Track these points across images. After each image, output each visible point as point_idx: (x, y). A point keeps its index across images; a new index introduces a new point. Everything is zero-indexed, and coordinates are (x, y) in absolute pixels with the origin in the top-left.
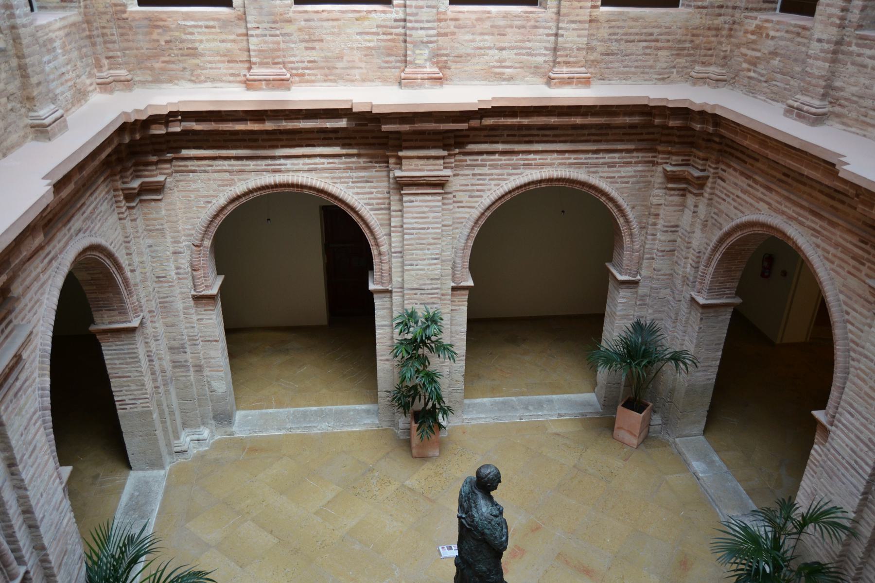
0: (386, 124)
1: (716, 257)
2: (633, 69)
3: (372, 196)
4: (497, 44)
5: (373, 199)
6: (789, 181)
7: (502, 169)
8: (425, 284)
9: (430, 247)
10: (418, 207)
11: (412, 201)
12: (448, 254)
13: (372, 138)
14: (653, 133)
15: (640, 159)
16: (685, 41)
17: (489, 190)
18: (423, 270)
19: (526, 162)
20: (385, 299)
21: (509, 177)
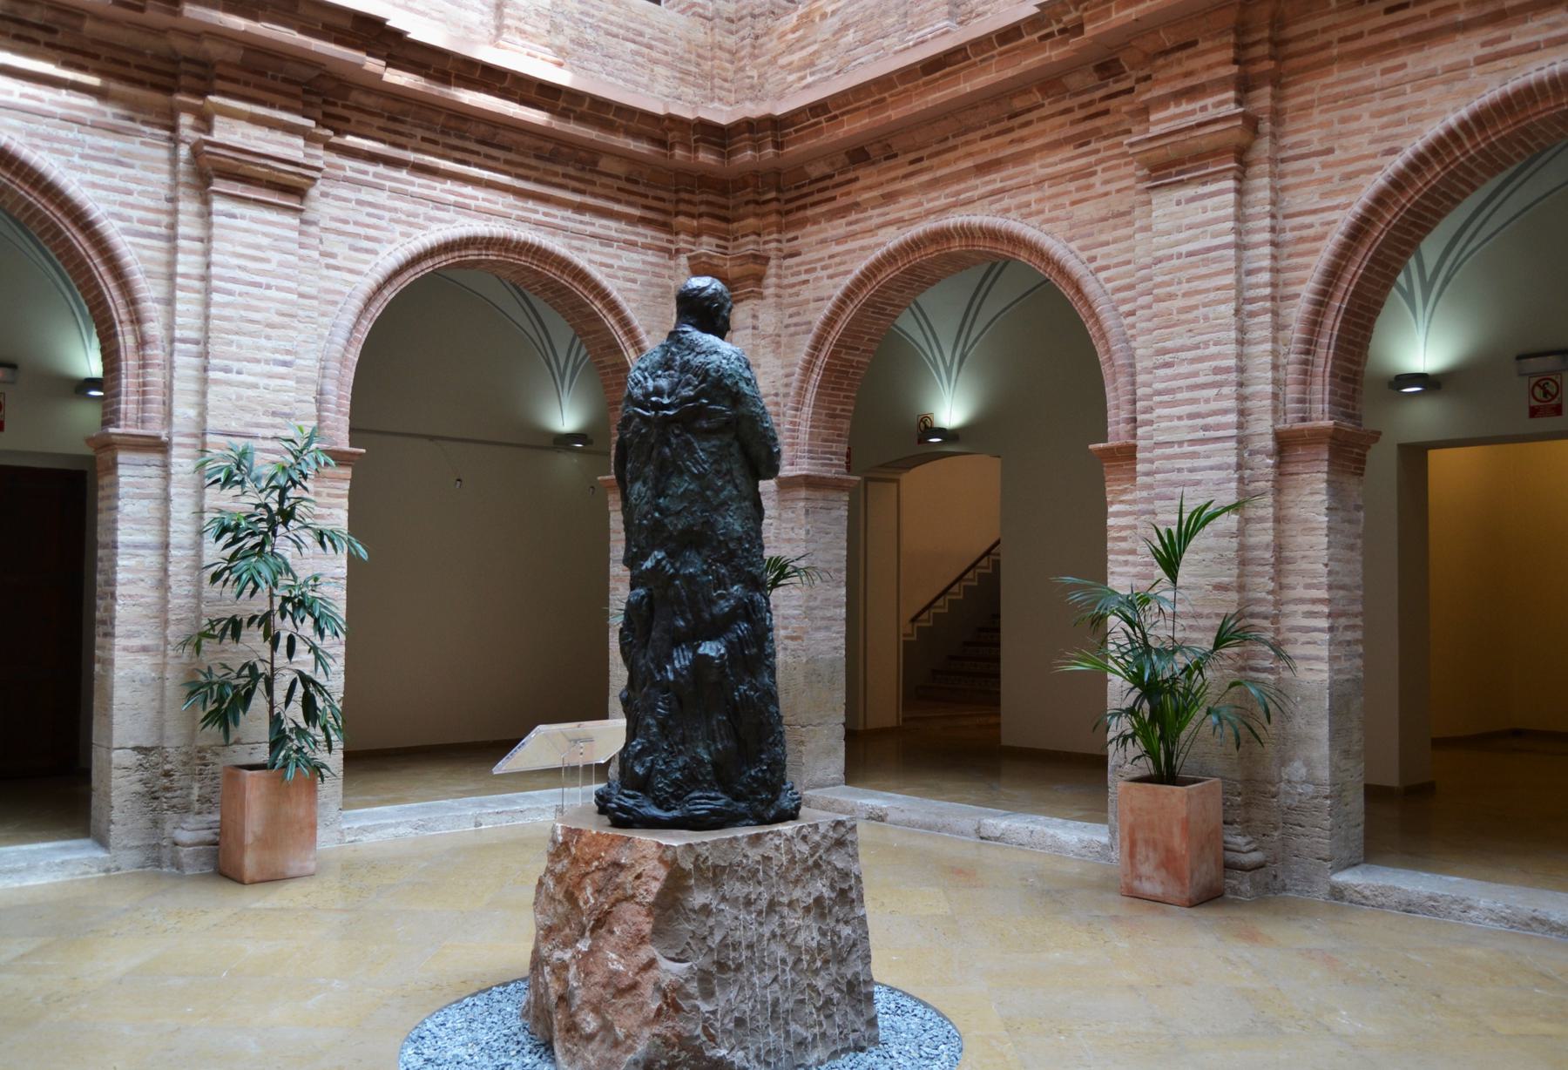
1: (812, 382)
2: (621, 83)
3: (130, 199)
5: (133, 206)
6: (926, 163)
7: (414, 202)
8: (258, 425)
10: (246, 231)
11: (233, 216)
12: (308, 363)
13: (138, 67)
15: (649, 241)
16: (689, 61)
17: (391, 242)
18: (255, 386)
20: (148, 471)
21: (428, 223)
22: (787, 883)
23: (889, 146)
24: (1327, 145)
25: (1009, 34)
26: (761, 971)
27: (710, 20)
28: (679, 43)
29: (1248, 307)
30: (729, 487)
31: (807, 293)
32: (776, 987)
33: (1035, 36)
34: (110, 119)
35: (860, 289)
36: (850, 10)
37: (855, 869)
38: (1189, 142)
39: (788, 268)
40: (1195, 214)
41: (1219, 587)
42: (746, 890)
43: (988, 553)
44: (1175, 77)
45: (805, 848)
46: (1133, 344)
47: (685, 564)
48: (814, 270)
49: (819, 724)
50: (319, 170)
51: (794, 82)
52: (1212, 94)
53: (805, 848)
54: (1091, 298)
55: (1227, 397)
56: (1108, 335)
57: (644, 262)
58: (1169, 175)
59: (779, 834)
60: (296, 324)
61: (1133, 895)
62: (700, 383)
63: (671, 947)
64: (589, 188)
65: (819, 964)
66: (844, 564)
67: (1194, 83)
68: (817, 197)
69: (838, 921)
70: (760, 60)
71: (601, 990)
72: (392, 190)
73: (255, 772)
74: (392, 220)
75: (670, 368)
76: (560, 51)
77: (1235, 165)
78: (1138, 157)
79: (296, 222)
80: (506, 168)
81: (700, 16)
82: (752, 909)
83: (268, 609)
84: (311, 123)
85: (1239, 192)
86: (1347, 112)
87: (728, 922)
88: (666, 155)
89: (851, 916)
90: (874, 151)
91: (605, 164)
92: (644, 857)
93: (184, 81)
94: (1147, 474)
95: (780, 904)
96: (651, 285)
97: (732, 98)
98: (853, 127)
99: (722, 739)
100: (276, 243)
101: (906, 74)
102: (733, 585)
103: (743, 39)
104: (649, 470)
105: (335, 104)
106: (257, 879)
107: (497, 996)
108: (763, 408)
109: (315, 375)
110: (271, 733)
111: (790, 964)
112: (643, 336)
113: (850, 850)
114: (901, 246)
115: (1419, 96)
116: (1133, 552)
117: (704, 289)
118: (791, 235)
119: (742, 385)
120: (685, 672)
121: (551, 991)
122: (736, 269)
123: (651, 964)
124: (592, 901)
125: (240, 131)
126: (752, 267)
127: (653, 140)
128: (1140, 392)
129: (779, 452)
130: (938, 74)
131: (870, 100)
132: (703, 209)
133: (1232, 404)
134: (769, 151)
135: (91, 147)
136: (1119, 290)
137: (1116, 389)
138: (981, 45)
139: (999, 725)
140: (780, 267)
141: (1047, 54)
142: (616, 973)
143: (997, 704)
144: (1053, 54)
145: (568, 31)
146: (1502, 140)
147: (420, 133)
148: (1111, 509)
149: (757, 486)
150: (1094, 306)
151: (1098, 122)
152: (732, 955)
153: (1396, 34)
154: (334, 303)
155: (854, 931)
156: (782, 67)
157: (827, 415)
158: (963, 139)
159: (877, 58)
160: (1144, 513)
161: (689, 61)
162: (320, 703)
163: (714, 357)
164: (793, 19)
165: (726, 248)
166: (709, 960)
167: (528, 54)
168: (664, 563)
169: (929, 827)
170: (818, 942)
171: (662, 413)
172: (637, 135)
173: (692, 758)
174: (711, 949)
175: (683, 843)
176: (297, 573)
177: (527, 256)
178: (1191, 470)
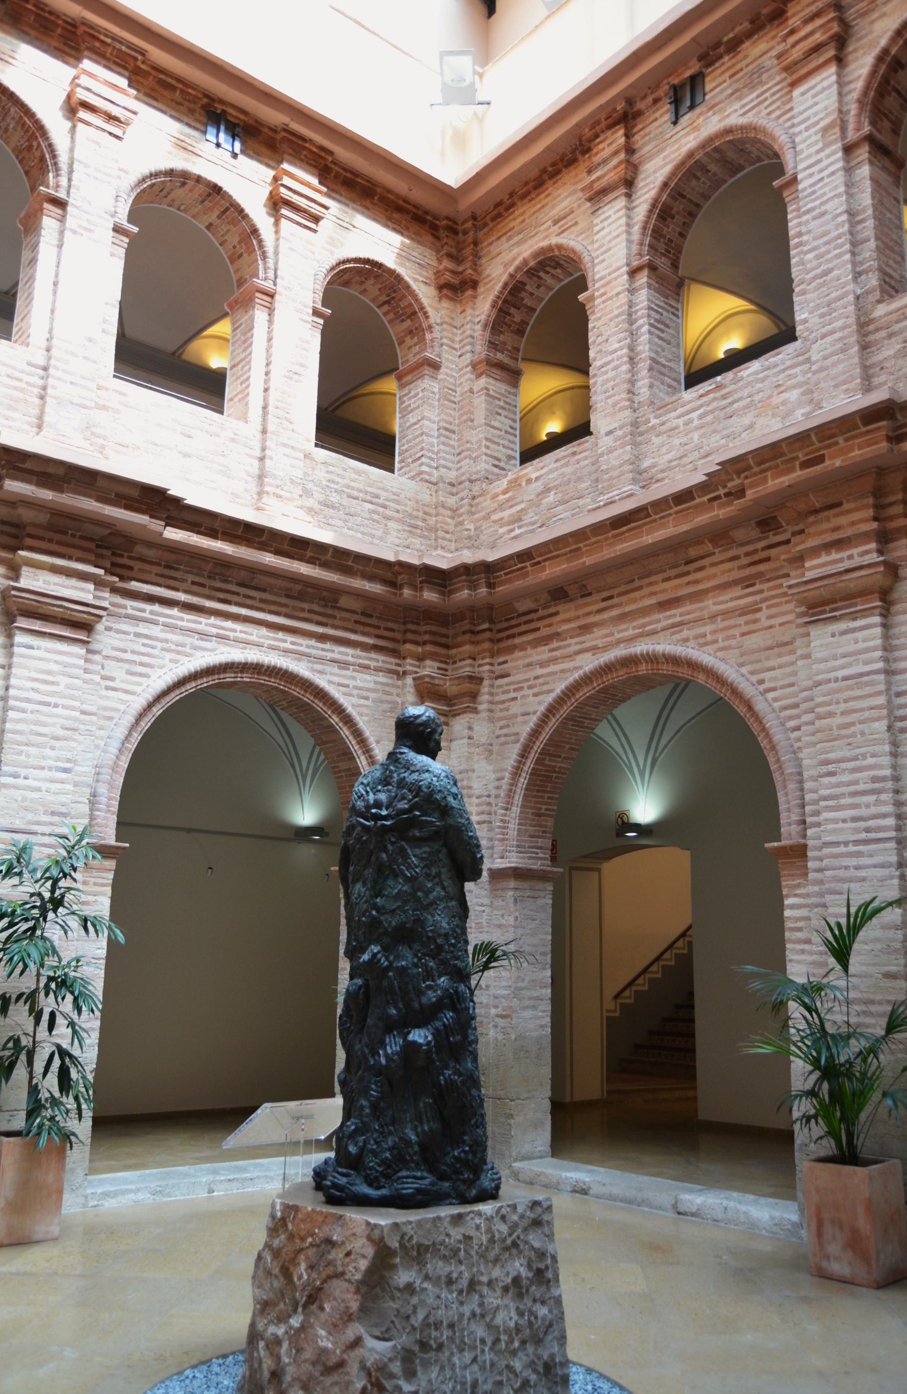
0: (14, 478)
1: (520, 785)
2: (360, 535)
6: (616, 600)
8: (38, 823)
9: (57, 744)
10: (41, 659)
11: (31, 647)
12: (85, 771)
14: (392, 630)
15: (380, 664)
16: (417, 517)
17: (161, 667)
18: (39, 790)
19: (222, 632)
21: (194, 652)
22: (487, 1262)
23: (584, 586)
25: (683, 497)
26: (461, 1351)
27: (436, 484)
29: (899, 724)
30: (438, 889)
31: (515, 708)
32: (475, 1368)
33: (705, 498)
35: (561, 705)
36: (551, 476)
37: (550, 1249)
39: (499, 687)
40: (847, 644)
41: (888, 975)
42: (448, 1269)
43: (683, 935)
45: (504, 1228)
46: (800, 755)
47: (398, 957)
48: (521, 688)
49: (527, 1098)
50: (105, 609)
51: (504, 534)
52: (856, 546)
53: (504, 1228)
54: (761, 715)
55: (885, 803)
56: (778, 747)
57: (376, 682)
58: (824, 612)
59: (479, 1214)
60: (76, 736)
61: (823, 1275)
62: (414, 797)
63: (377, 1325)
64: (330, 621)
65: (516, 1344)
66: (549, 948)
67: (841, 536)
68: (523, 628)
69: (535, 1301)
70: (476, 516)
71: (310, 1367)
72: (165, 625)
73: (12, 1139)
74: (163, 649)
75: (388, 784)
78: (796, 597)
79: (83, 651)
80: (262, 605)
81: (427, 481)
82: (454, 1287)
83: (34, 987)
84: (101, 572)
85: (884, 626)
87: (431, 1301)
88: (395, 594)
89: (548, 1296)
90: (572, 590)
91: (344, 601)
92: (354, 1235)
94: (819, 870)
95: (480, 1283)
96: (381, 702)
97: (453, 546)
98: (553, 571)
99: (428, 1121)
100: (66, 669)
101: (598, 529)
102: (440, 977)
103: (462, 499)
104: (369, 873)
105: (122, 556)
106: (5, 1242)
107: (216, 1369)
108: (468, 819)
109: (90, 780)
110: (28, 1103)
111: (489, 1343)
112: (374, 746)
113: (546, 1230)
114: (596, 670)
116: (808, 941)
117: (419, 716)
118: (501, 659)
119: (450, 799)
120: (395, 1057)
121: (265, 1366)
122: (455, 688)
123: (357, 1342)
124: (305, 1277)
125: (42, 578)
126: (467, 686)
127: (385, 582)
128: (808, 797)
129: (482, 857)
130: (624, 529)
132: (427, 637)
133: (889, 809)
134: (483, 590)
136: (785, 708)
137: (786, 795)
138: (660, 505)
139: (695, 1099)
140: (492, 686)
141: (716, 513)
142: (324, 1351)
143: (694, 1077)
144: (721, 512)
145: (317, 495)
147: (190, 578)
148: (788, 902)
149: (463, 887)
150: (764, 722)
151: (761, 568)
152: (434, 1334)
154: (111, 718)
155: (550, 1311)
156: (495, 522)
157: (533, 814)
158: (647, 580)
159: (573, 515)
160: (817, 906)
161: (417, 517)
162: (74, 1074)
163: (427, 775)
164: (504, 483)
165: (446, 670)
166: (412, 1339)
168: (379, 956)
169: (630, 1202)
170: (516, 1324)
171: (380, 823)
172: (371, 578)
173: (401, 1139)
174: (414, 1328)
175: (390, 1221)
176: (61, 954)
177: (275, 678)
178: (857, 868)
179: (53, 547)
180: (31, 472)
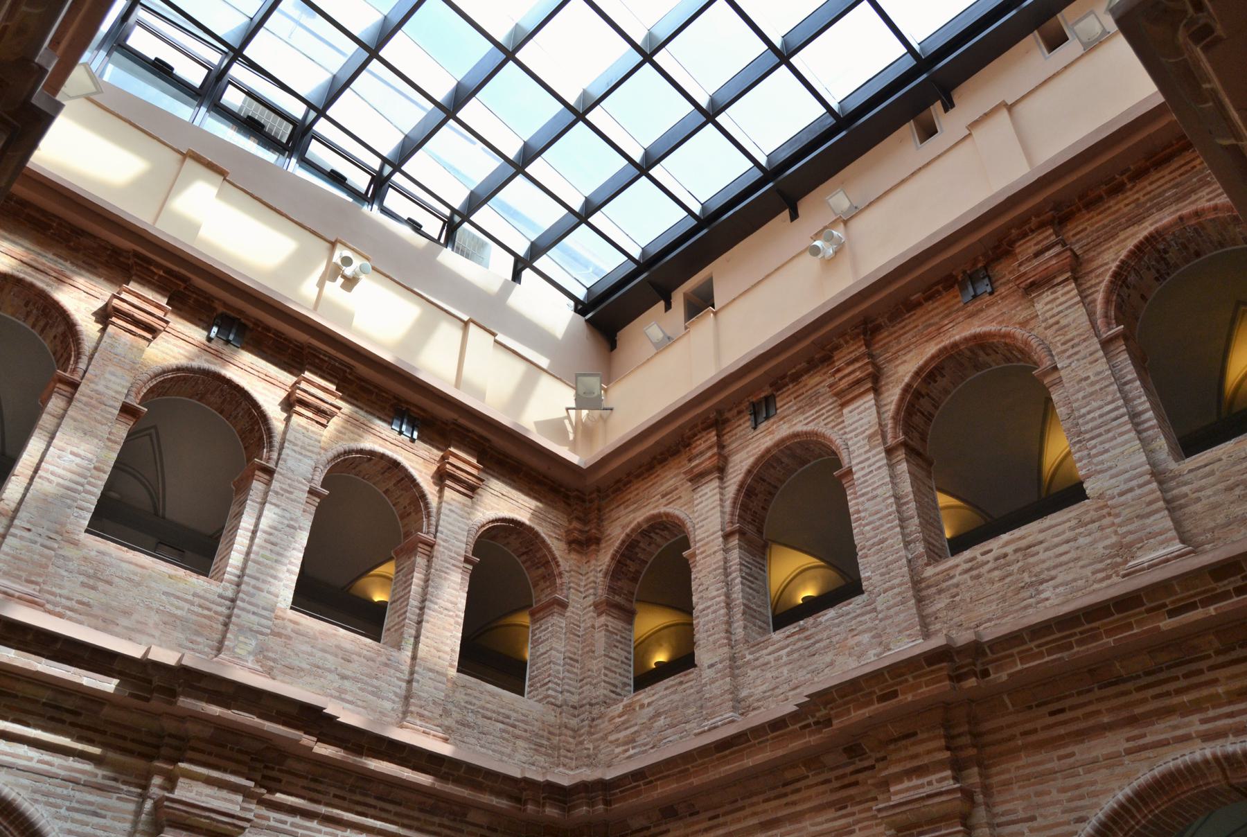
0: (188, 695)
2: (491, 753)
4: (339, 668)
6: (721, 820)
13: (133, 740)
16: (542, 737)
24: (1029, 814)
25: (777, 725)
28: (536, 723)
33: (798, 726)
34: (99, 780)
36: (661, 702)
38: (923, 810)
44: (905, 759)
50: (248, 820)
51: (619, 753)
67: (920, 763)
76: (447, 729)
77: (961, 828)
78: (886, 820)
80: (395, 819)
81: (552, 704)
84: (251, 784)
86: (1039, 788)
91: (473, 816)
93: (164, 751)
97: (573, 764)
98: (664, 790)
101: (703, 751)
103: (583, 721)
105: (273, 769)
115: (1089, 777)
125: (195, 789)
127: (510, 797)
130: (727, 752)
131: (677, 770)
134: (601, 807)
135: (78, 802)
138: (758, 732)
141: (807, 739)
144: (812, 739)
145: (455, 715)
146: (1163, 812)
147: (333, 791)
151: (852, 791)
153: (1062, 731)
156: (611, 742)
164: (619, 707)
167: (424, 732)
172: (499, 794)
179: (212, 760)
180: (205, 690)
